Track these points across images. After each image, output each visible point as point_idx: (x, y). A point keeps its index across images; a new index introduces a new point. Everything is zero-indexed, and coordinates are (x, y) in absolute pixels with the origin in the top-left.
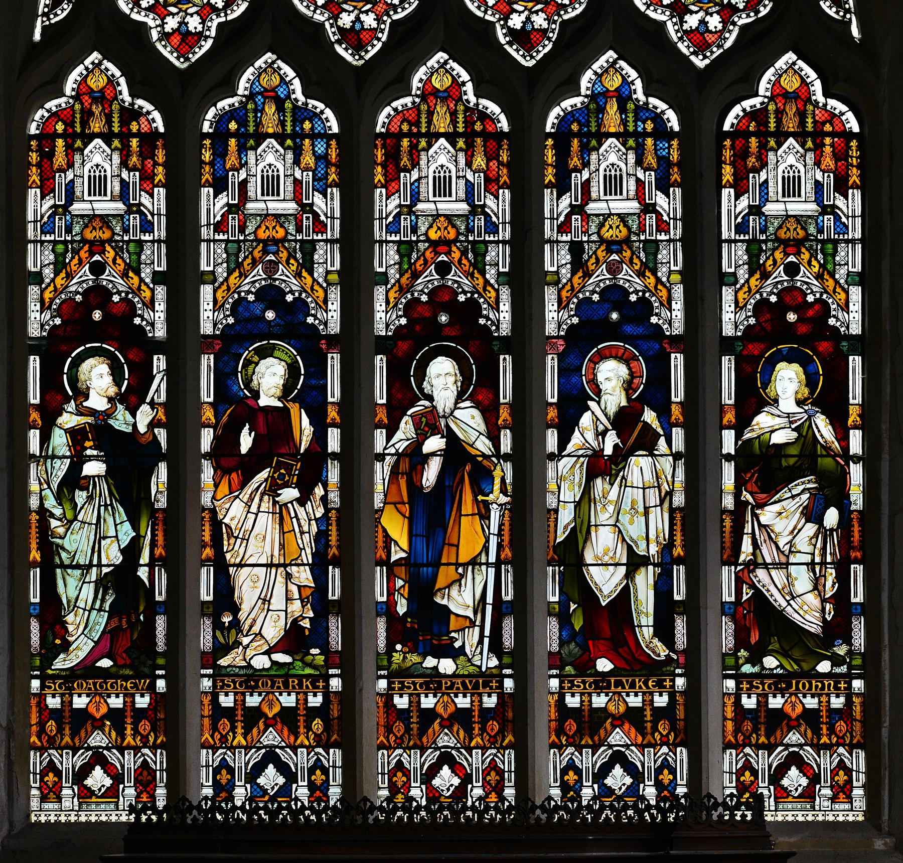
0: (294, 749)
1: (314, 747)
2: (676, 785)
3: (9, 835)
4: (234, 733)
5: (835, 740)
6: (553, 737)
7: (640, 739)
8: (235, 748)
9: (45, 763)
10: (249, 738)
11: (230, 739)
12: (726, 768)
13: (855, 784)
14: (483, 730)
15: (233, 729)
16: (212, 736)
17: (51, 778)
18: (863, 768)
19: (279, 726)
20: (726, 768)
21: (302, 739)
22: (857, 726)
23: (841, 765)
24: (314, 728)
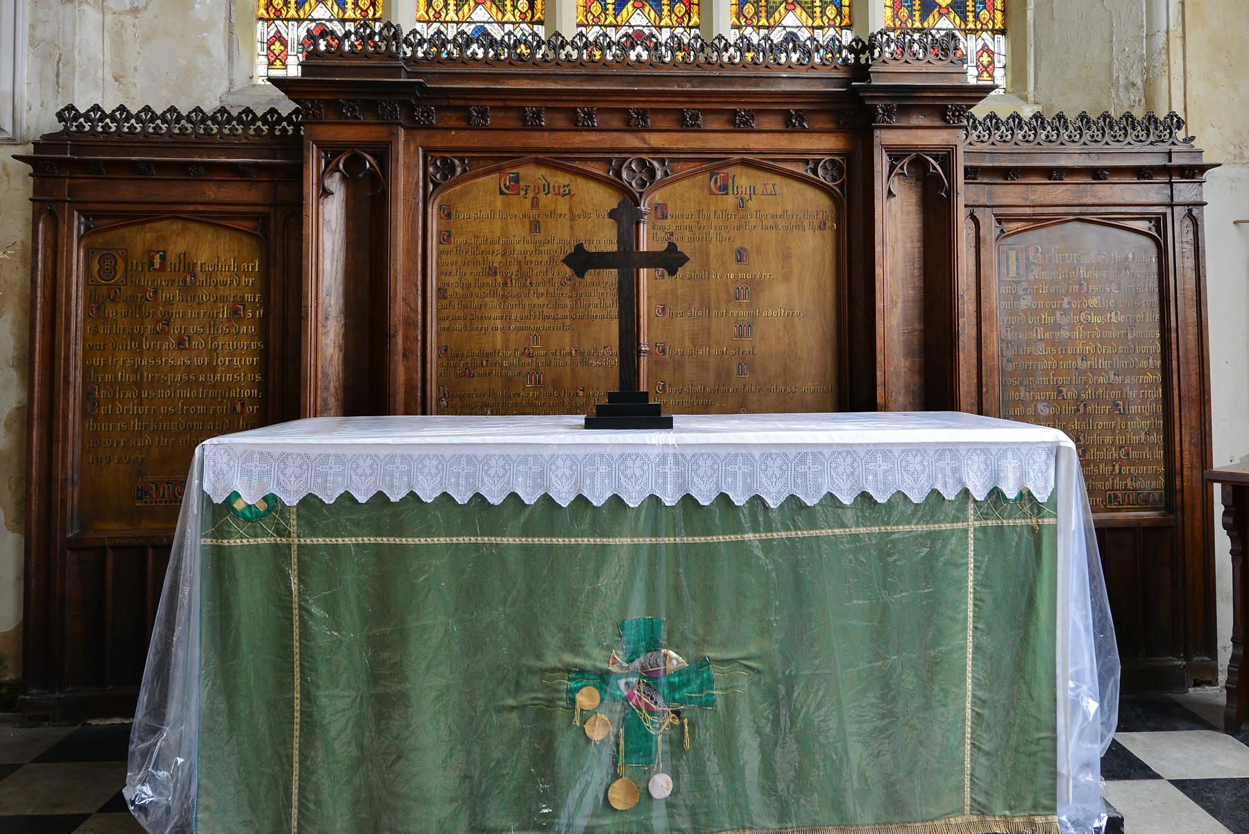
0: (502, 24)
1: (274, 20)
2: (287, 55)
3: (229, 92)
4: (447, 10)
5: (979, 26)
6: (734, 19)
7: (810, 23)
8: (447, 22)
9: (272, 34)
10: (460, 14)
11: (443, 15)
12: (259, 37)
13: (997, 65)
14: (671, 11)
15: (911, 16)
16: (427, 12)
17: (277, 47)
18: (1003, 52)
19: (952, 16)
20: (259, 37)
21: (509, 16)
22: (999, 15)
23: (985, 48)
24: (828, 13)
